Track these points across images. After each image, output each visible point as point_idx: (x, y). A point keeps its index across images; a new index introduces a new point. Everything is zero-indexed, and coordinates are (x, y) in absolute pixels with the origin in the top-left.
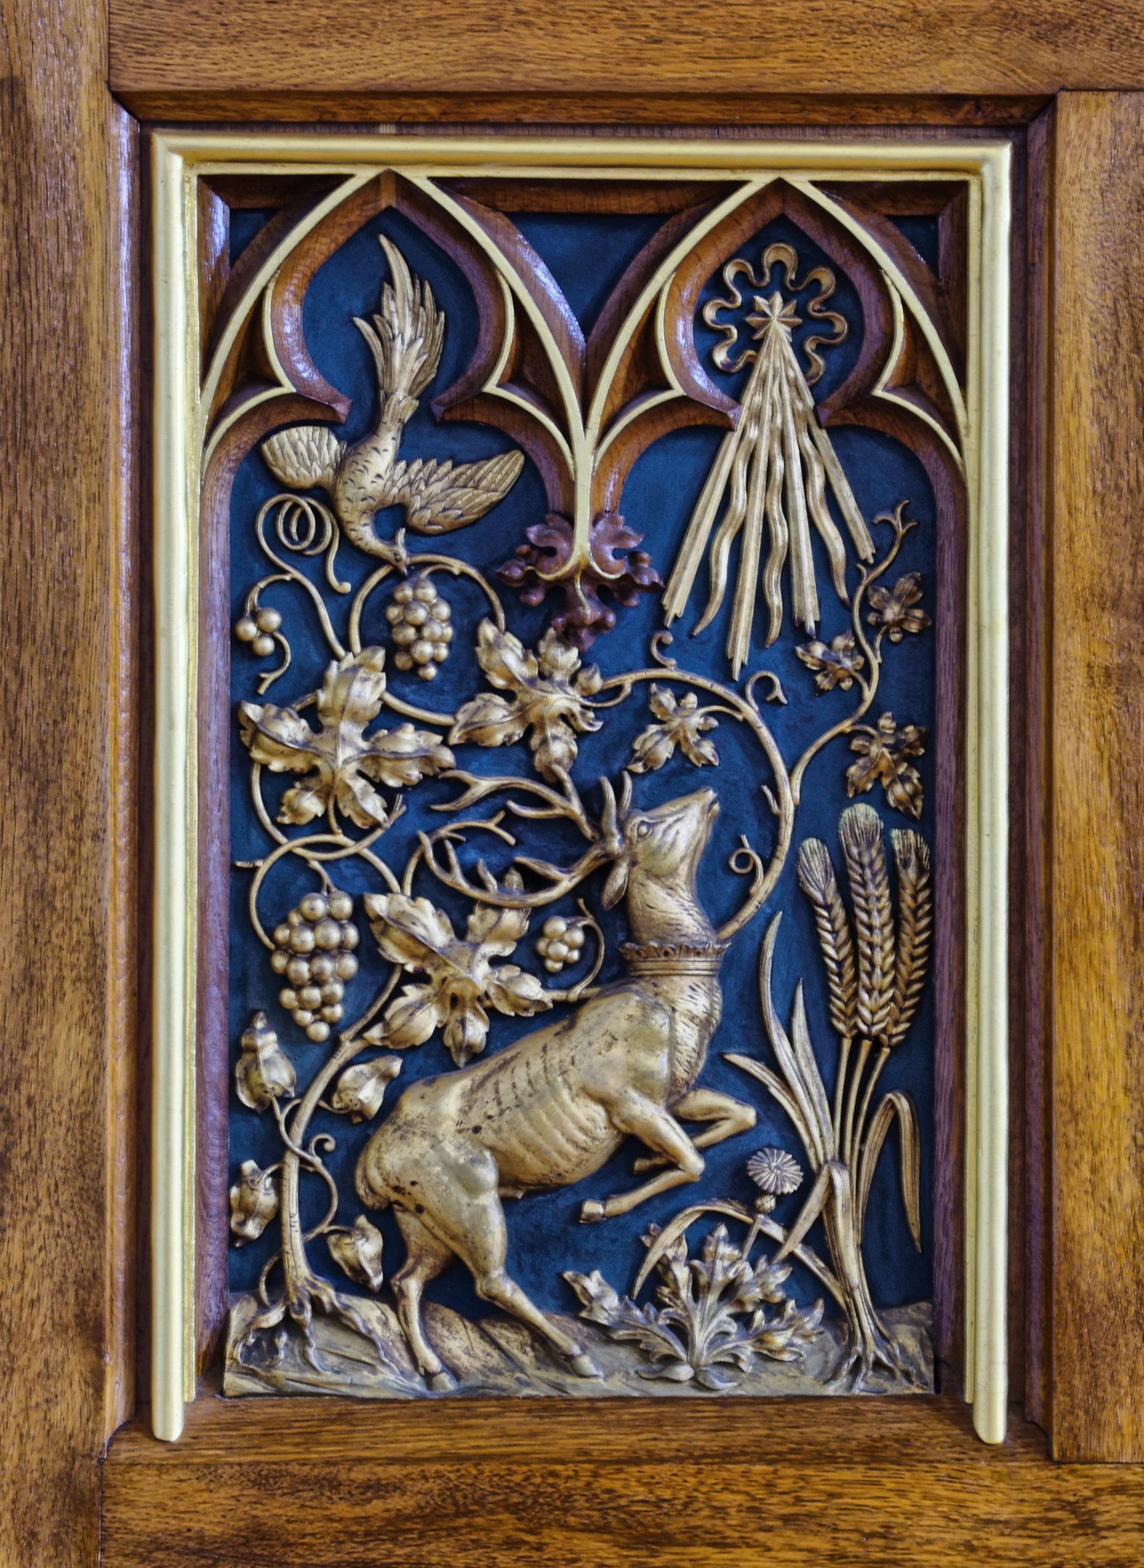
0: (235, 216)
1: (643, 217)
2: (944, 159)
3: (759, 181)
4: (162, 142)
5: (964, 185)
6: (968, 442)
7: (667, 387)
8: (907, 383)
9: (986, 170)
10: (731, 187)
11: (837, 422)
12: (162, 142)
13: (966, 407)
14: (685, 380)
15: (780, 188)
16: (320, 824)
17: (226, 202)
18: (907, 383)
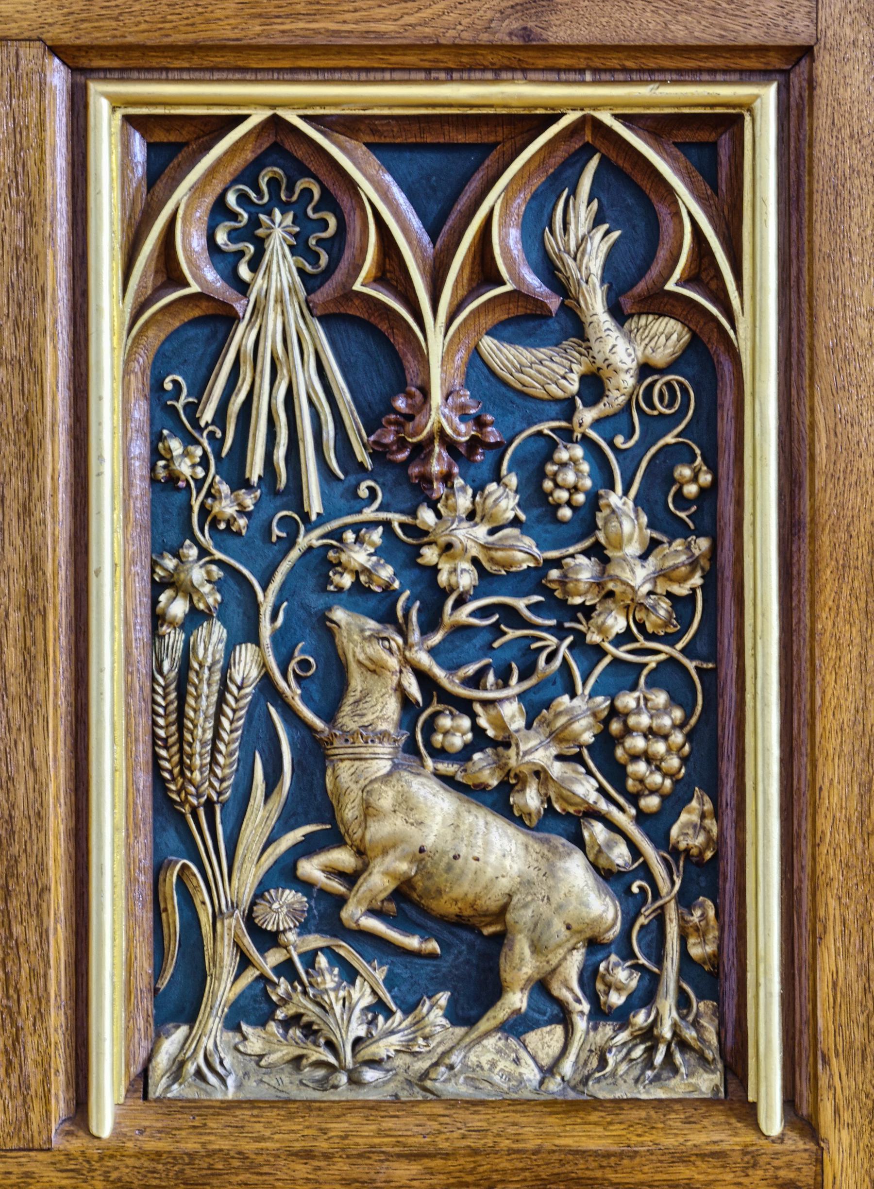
0: (151, 147)
1: (170, 144)
2: (215, 95)
3: (258, 117)
4: (96, 88)
5: (741, 117)
6: (743, 324)
7: (187, 285)
8: (381, 279)
9: (757, 104)
10: (554, 118)
11: (333, 309)
12: (96, 88)
13: (741, 295)
14: (200, 280)
15: (275, 123)
16: (625, 637)
17: (143, 136)
18: (381, 279)
